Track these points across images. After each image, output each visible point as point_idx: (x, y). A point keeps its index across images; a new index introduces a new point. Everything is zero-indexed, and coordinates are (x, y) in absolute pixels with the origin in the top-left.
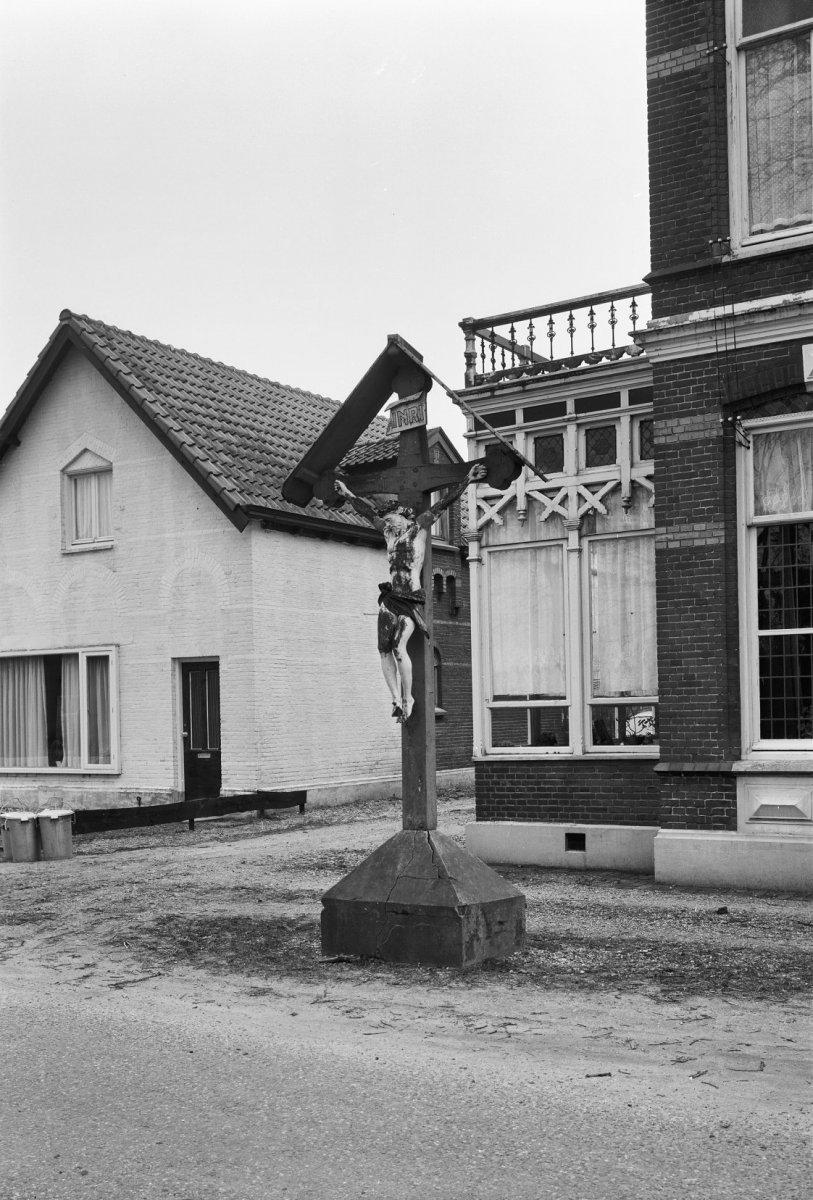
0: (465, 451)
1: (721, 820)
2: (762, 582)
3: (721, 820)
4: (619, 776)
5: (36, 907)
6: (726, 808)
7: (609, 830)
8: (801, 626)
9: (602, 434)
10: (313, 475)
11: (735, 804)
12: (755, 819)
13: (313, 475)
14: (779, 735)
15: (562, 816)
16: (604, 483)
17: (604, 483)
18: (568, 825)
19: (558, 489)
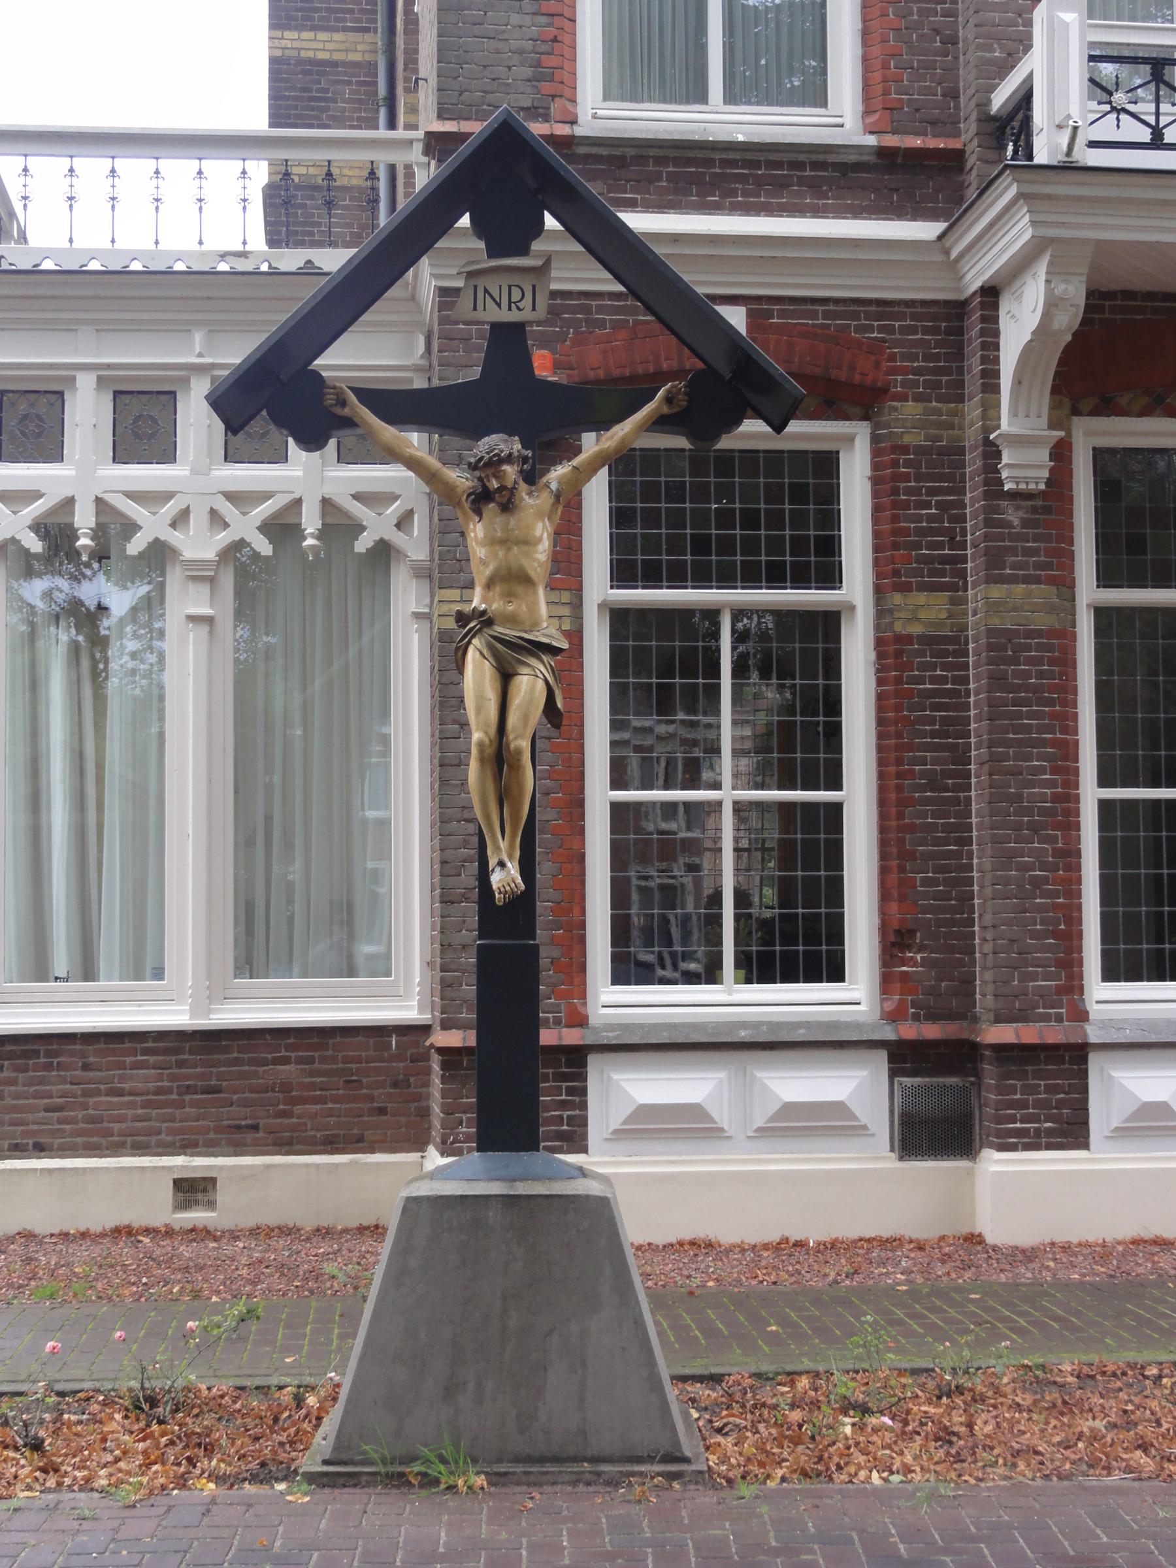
0: (726, 443)
1: (561, 1136)
2: (833, 705)
3: (561, 1136)
4: (286, 1061)
5: (946, 1356)
6: (566, 1114)
7: (268, 1167)
8: (1125, 784)
9: (32, 405)
10: (192, 432)
11: (584, 1106)
12: (620, 1135)
13: (192, 432)
14: (1134, 975)
15: (160, 1144)
16: (267, 496)
17: (267, 496)
18: (179, 1160)
19: (168, 496)
